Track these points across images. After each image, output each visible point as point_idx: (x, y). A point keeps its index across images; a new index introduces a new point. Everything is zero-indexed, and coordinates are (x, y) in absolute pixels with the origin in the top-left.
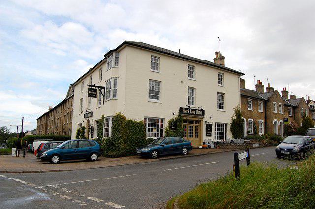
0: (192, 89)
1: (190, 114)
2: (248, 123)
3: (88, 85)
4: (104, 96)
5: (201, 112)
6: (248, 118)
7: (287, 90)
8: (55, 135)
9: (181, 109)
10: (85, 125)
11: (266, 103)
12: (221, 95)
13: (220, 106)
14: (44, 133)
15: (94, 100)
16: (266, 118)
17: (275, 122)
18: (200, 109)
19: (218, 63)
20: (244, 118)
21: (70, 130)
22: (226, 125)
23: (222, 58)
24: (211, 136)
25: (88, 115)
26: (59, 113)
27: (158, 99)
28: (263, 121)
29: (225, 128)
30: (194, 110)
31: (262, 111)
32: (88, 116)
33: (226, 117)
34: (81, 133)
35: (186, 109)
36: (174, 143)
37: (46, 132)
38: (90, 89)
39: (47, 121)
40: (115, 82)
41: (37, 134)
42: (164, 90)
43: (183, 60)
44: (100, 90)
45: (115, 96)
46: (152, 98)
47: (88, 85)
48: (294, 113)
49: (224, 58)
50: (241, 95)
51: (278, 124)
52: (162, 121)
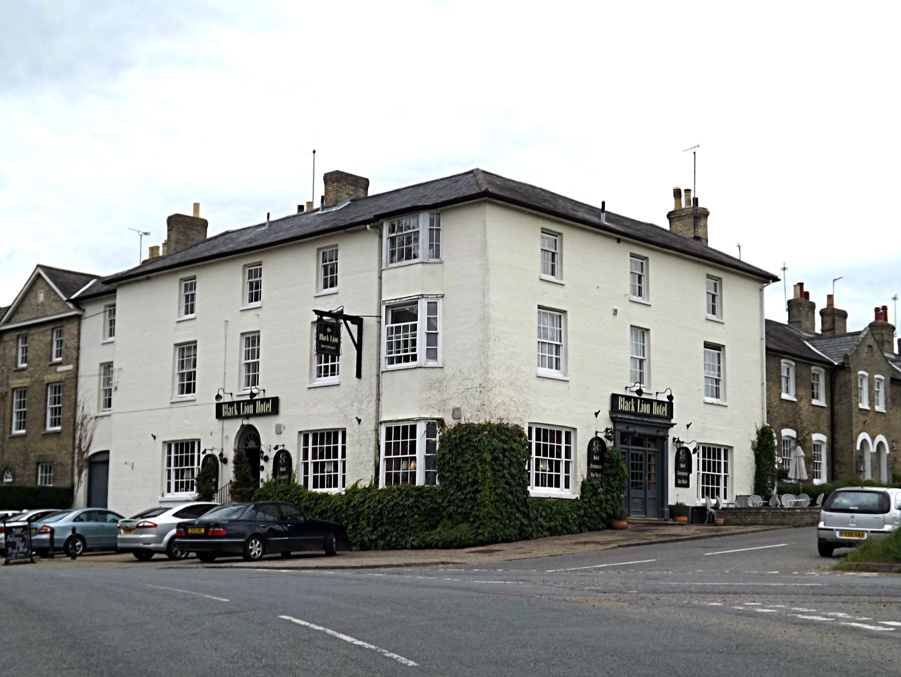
9: (615, 397)
13: (553, 353)
16: (832, 432)
19: (685, 230)
22: (568, 435)
23: (699, 215)
24: (687, 486)
28: (823, 438)
35: (628, 398)
40: (432, 308)
45: (432, 354)
49: (705, 214)
50: (767, 349)
51: (873, 449)
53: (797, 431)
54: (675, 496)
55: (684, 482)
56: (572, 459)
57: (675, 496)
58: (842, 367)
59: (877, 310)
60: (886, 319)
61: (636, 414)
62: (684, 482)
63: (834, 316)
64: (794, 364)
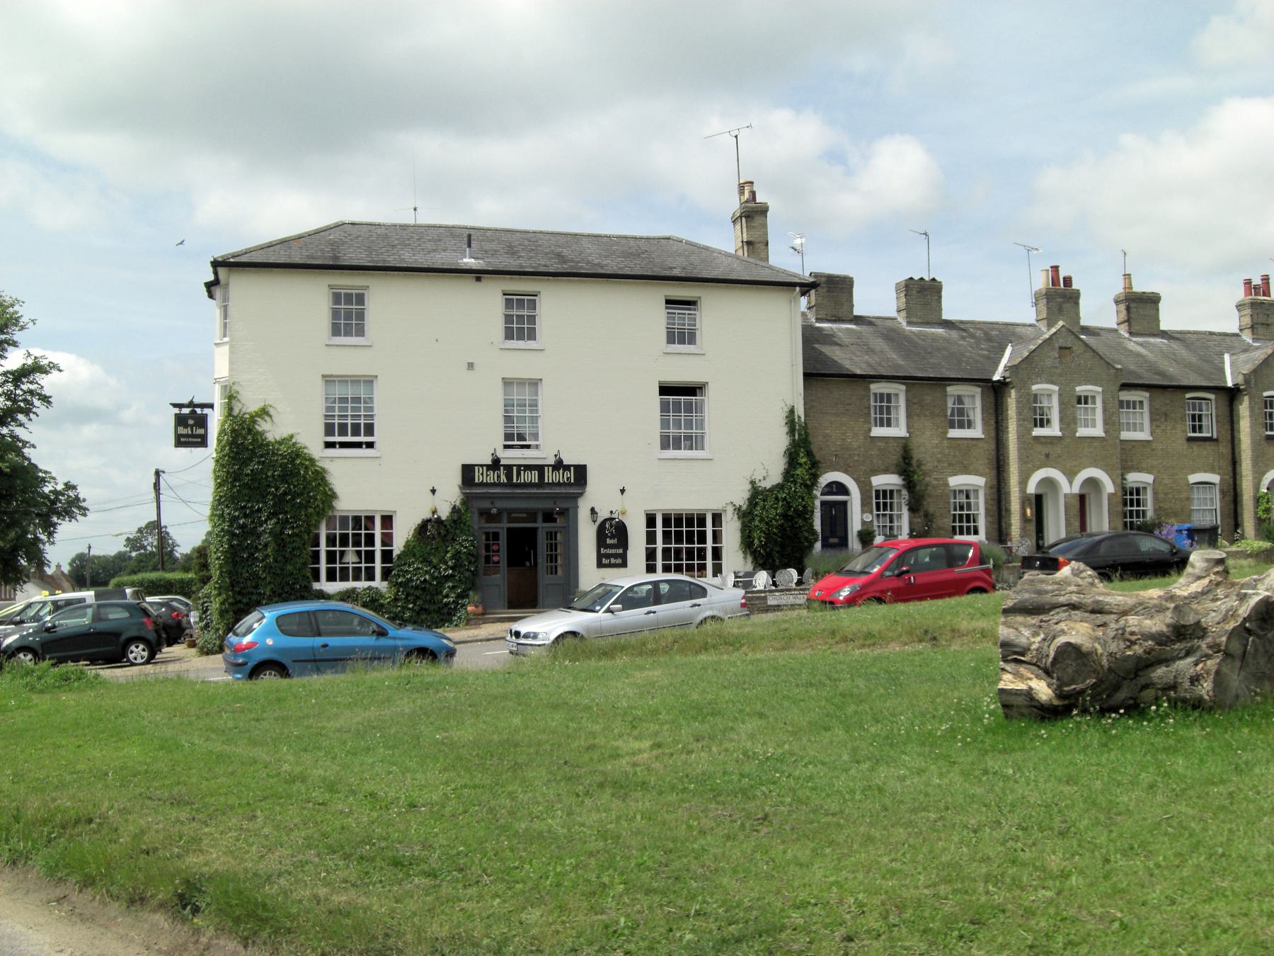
3: (175, 405)
6: (876, 472)
9: (468, 471)
31: (977, 432)
36: (714, 532)
43: (478, 279)
47: (175, 405)
52: (387, 520)
55: (619, 561)
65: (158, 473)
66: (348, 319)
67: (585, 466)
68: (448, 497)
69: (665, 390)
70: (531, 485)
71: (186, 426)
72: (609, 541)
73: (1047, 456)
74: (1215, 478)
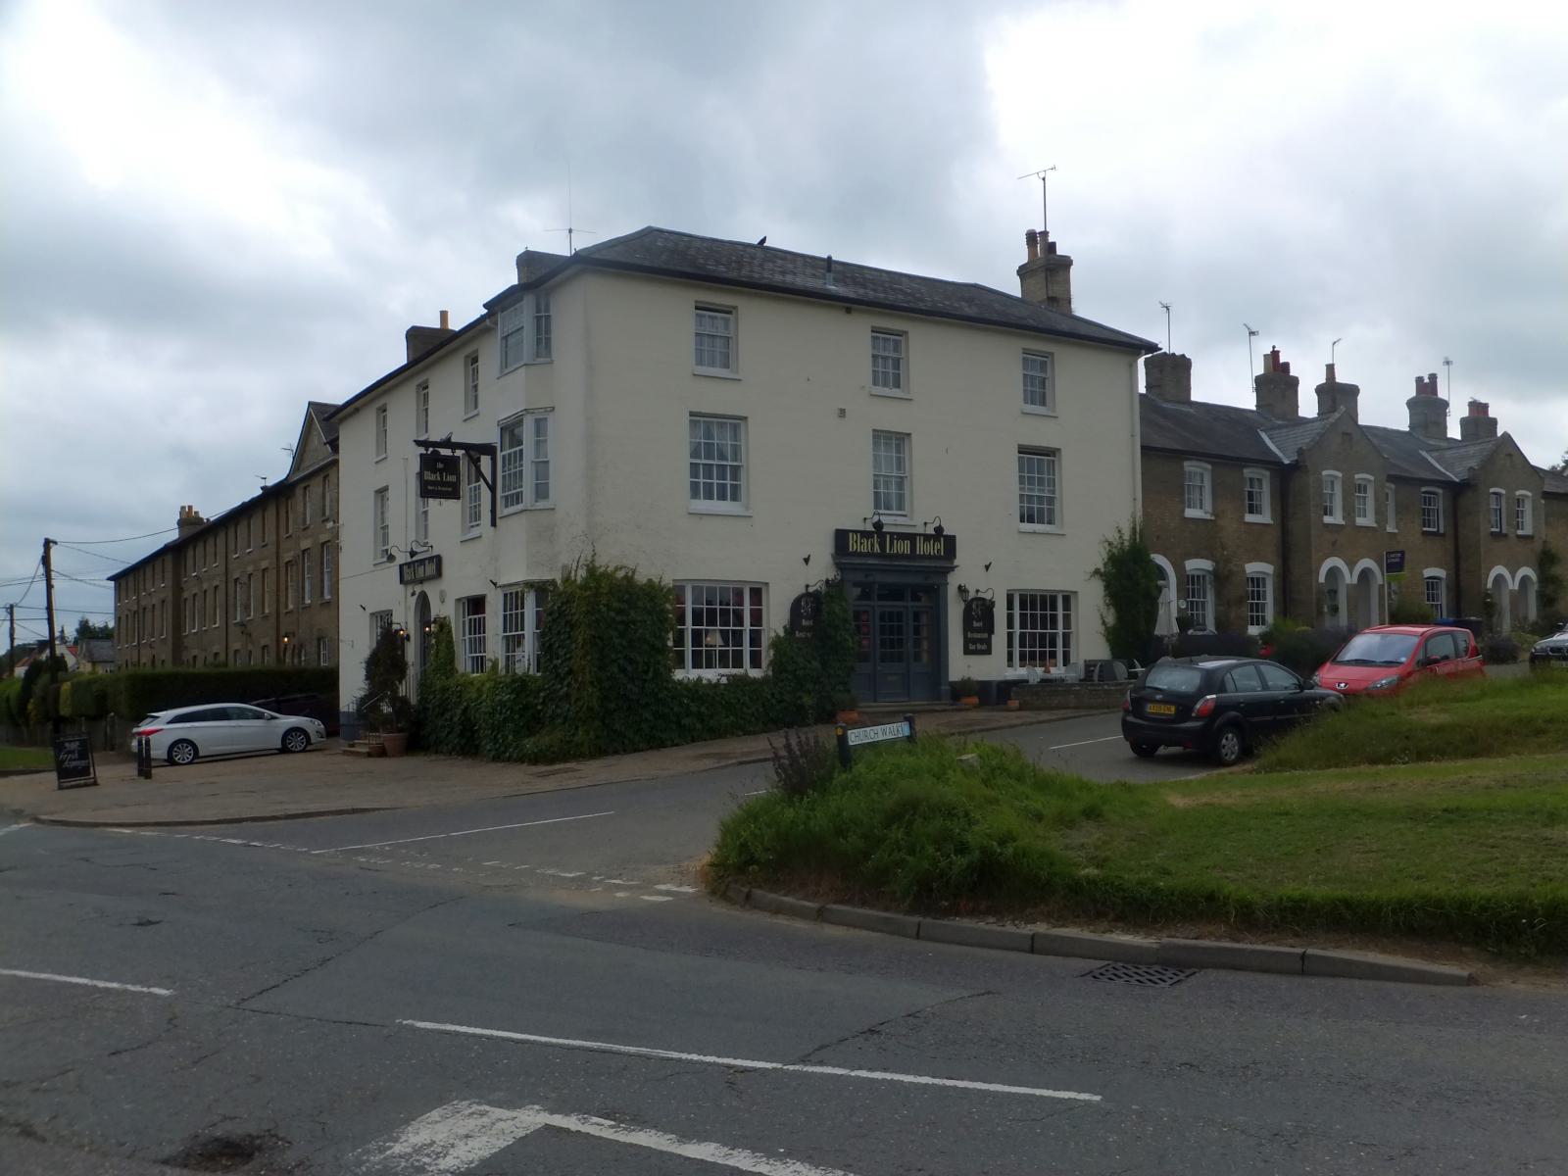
0: (893, 442)
1: (891, 557)
2: (1189, 585)
3: (419, 443)
4: (493, 488)
5: (941, 546)
7: (1442, 394)
8: (238, 665)
9: (841, 536)
10: (405, 619)
11: (1288, 478)
12: (1038, 461)
13: (1037, 511)
14: (165, 654)
15: (445, 513)
17: (1333, 573)
18: (930, 530)
20: (1159, 559)
21: (328, 640)
22: (1067, 599)
24: (988, 652)
25: (421, 569)
26: (250, 550)
27: (735, 497)
29: (1060, 612)
30: (902, 536)
31: (1265, 517)
32: (421, 573)
33: (1070, 562)
34: (387, 657)
35: (865, 534)
37: (178, 645)
38: (429, 462)
39: (178, 588)
41: (155, 654)
42: (762, 456)
43: (848, 311)
44: (476, 462)
45: (542, 492)
46: (709, 496)
48: (1455, 515)
52: (757, 594)
53: (1217, 562)
54: (961, 666)
55: (984, 647)
56: (1073, 629)
57: (961, 666)
58: (1295, 467)
59: (1419, 380)
60: (1435, 392)
61: (883, 555)
62: (984, 647)
63: (1337, 395)
64: (1209, 467)
65: (48, 544)
66: (716, 350)
67: (954, 537)
68: (821, 571)
69: (1023, 450)
70: (903, 557)
71: (434, 471)
72: (976, 624)
73: (1334, 543)
74: (1441, 573)
